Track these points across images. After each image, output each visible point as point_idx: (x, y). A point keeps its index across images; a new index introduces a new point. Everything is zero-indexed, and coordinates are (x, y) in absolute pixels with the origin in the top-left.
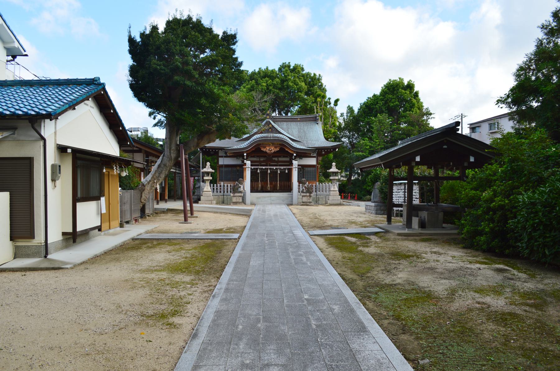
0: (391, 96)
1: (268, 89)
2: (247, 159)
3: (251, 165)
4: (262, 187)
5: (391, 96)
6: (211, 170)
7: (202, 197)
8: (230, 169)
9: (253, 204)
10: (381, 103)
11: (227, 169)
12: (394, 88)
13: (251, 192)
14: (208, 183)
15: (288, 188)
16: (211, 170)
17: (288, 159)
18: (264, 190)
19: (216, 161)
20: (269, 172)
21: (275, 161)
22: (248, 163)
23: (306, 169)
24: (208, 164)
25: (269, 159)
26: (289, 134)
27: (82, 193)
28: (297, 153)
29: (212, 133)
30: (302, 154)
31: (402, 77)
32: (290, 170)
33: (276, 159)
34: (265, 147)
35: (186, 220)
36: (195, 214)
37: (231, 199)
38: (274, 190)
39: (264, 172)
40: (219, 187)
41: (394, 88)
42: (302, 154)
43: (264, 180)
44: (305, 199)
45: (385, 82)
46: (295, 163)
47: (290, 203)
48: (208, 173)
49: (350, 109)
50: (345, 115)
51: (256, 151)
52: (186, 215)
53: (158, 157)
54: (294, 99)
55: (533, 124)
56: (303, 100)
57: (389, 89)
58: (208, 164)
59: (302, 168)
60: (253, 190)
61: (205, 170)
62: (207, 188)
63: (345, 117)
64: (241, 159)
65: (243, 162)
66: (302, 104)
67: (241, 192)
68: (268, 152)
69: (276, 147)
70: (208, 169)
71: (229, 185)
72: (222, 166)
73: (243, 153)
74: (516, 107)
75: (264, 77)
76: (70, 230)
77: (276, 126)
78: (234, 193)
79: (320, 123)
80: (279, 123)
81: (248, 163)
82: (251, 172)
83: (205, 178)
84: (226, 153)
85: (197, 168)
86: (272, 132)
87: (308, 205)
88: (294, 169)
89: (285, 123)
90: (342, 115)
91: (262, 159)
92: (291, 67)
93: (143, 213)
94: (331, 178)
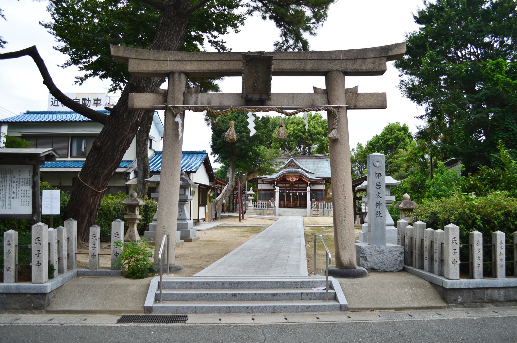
0: (389, 136)
1: (294, 132)
2: (277, 186)
4: (287, 204)
5: (389, 136)
6: (253, 193)
7: (247, 211)
8: (265, 192)
9: (280, 215)
10: (381, 142)
11: (263, 192)
12: (392, 130)
14: (251, 201)
15: (304, 206)
16: (253, 193)
17: (305, 185)
18: (288, 207)
19: (256, 186)
20: (291, 194)
21: (296, 187)
22: (277, 188)
23: (318, 192)
24: (251, 188)
25: (292, 185)
26: (306, 168)
27: (202, 202)
28: (310, 181)
29: (256, 172)
31: (398, 122)
32: (306, 194)
33: (297, 185)
34: (289, 178)
35: (240, 220)
36: (245, 218)
37: (266, 212)
38: (295, 207)
39: (288, 194)
40: (258, 204)
41: (392, 130)
42: (314, 182)
43: (288, 199)
44: (314, 213)
45: (386, 125)
46: (308, 188)
47: (304, 215)
48: (251, 195)
49: (360, 146)
50: (355, 150)
51: (283, 180)
52: (241, 218)
53: (225, 185)
54: (314, 140)
56: (321, 141)
57: (388, 131)
58: (251, 188)
59: (313, 192)
60: (281, 206)
61: (249, 192)
62: (250, 204)
63: (356, 152)
64: (273, 185)
65: (274, 187)
66: (320, 143)
67: (272, 207)
68: (291, 181)
69: (296, 178)
70: (251, 192)
71: (264, 202)
72: (260, 190)
73: (274, 181)
75: (292, 123)
76: (197, 218)
77: (297, 163)
78: (268, 207)
79: (329, 160)
80: (300, 160)
81: (277, 188)
83: (249, 198)
84: (263, 181)
85: (243, 191)
86: (294, 168)
89: (304, 160)
90: (353, 150)
92: (312, 116)
93: (216, 218)
94: (57, 159)
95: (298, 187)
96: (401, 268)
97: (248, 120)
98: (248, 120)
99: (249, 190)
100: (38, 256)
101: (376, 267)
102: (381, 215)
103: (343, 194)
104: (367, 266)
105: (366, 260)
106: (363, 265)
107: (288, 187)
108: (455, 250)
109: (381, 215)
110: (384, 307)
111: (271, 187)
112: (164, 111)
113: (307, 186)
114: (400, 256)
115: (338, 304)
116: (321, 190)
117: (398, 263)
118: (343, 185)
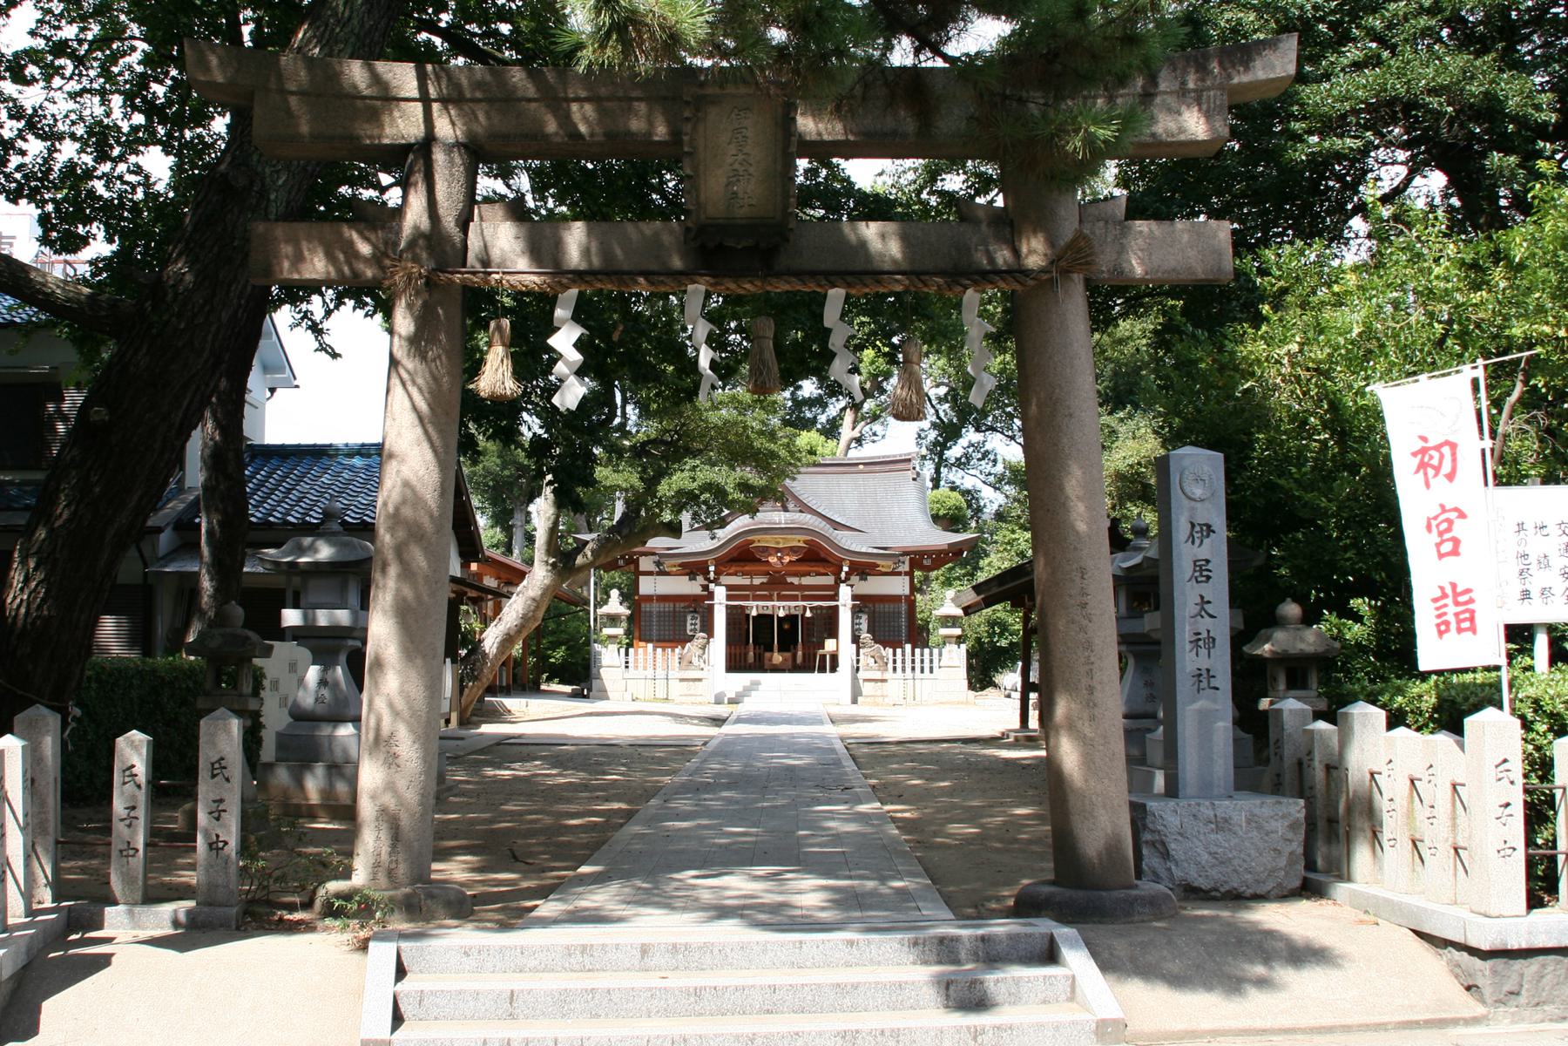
3: (729, 598)
13: (971, 687)
17: (829, 580)
18: (760, 666)
21: (792, 586)
22: (720, 593)
24: (615, 593)
30: (863, 568)
33: (795, 580)
42: (863, 568)
46: (845, 592)
55: (597, 451)
58: (615, 593)
61: (605, 610)
64: (700, 579)
65: (705, 588)
70: (615, 605)
72: (649, 598)
74: (525, 415)
81: (720, 593)
82: (728, 615)
84: (658, 564)
87: (1134, 737)
88: (716, 608)
91: (757, 581)
95: (801, 587)
96: (1297, 883)
97: (555, 341)
98: (555, 341)
99: (606, 602)
100: (218, 819)
101: (1202, 883)
102: (1214, 683)
103: (1084, 605)
104: (1171, 877)
105: (1166, 855)
106: (1155, 873)
107: (762, 586)
108: (1508, 805)
109: (1214, 683)
110: (1268, 1024)
111: (690, 587)
112: (1476, 370)
113: (838, 581)
114: (1290, 835)
115: (1085, 1016)
116: (895, 599)
117: (1283, 862)
118: (1083, 572)
